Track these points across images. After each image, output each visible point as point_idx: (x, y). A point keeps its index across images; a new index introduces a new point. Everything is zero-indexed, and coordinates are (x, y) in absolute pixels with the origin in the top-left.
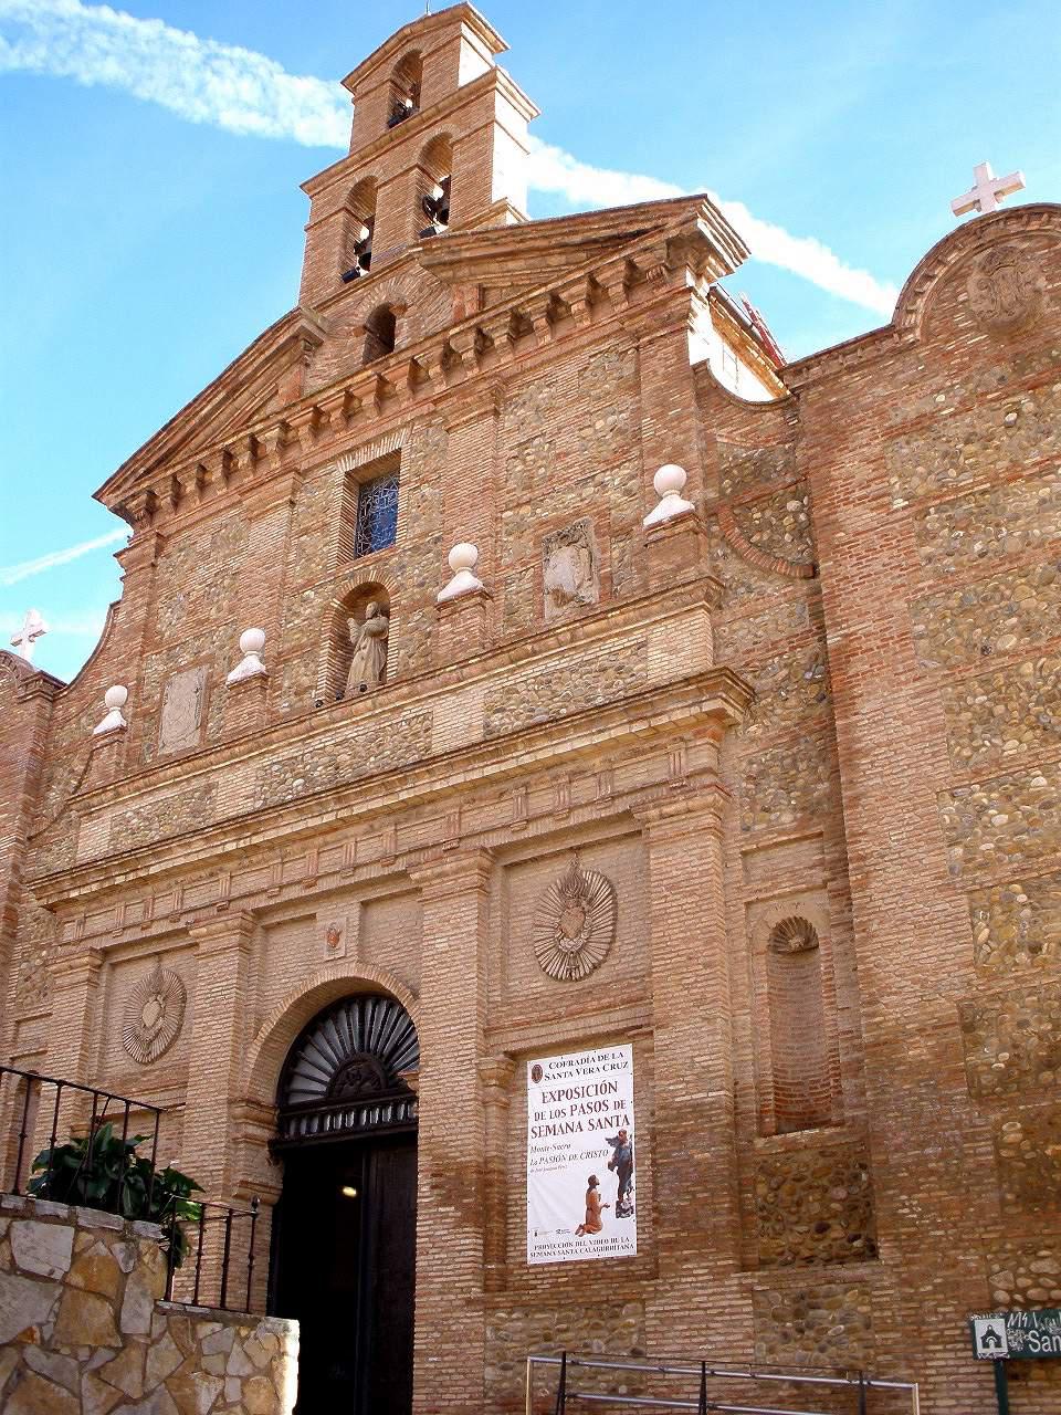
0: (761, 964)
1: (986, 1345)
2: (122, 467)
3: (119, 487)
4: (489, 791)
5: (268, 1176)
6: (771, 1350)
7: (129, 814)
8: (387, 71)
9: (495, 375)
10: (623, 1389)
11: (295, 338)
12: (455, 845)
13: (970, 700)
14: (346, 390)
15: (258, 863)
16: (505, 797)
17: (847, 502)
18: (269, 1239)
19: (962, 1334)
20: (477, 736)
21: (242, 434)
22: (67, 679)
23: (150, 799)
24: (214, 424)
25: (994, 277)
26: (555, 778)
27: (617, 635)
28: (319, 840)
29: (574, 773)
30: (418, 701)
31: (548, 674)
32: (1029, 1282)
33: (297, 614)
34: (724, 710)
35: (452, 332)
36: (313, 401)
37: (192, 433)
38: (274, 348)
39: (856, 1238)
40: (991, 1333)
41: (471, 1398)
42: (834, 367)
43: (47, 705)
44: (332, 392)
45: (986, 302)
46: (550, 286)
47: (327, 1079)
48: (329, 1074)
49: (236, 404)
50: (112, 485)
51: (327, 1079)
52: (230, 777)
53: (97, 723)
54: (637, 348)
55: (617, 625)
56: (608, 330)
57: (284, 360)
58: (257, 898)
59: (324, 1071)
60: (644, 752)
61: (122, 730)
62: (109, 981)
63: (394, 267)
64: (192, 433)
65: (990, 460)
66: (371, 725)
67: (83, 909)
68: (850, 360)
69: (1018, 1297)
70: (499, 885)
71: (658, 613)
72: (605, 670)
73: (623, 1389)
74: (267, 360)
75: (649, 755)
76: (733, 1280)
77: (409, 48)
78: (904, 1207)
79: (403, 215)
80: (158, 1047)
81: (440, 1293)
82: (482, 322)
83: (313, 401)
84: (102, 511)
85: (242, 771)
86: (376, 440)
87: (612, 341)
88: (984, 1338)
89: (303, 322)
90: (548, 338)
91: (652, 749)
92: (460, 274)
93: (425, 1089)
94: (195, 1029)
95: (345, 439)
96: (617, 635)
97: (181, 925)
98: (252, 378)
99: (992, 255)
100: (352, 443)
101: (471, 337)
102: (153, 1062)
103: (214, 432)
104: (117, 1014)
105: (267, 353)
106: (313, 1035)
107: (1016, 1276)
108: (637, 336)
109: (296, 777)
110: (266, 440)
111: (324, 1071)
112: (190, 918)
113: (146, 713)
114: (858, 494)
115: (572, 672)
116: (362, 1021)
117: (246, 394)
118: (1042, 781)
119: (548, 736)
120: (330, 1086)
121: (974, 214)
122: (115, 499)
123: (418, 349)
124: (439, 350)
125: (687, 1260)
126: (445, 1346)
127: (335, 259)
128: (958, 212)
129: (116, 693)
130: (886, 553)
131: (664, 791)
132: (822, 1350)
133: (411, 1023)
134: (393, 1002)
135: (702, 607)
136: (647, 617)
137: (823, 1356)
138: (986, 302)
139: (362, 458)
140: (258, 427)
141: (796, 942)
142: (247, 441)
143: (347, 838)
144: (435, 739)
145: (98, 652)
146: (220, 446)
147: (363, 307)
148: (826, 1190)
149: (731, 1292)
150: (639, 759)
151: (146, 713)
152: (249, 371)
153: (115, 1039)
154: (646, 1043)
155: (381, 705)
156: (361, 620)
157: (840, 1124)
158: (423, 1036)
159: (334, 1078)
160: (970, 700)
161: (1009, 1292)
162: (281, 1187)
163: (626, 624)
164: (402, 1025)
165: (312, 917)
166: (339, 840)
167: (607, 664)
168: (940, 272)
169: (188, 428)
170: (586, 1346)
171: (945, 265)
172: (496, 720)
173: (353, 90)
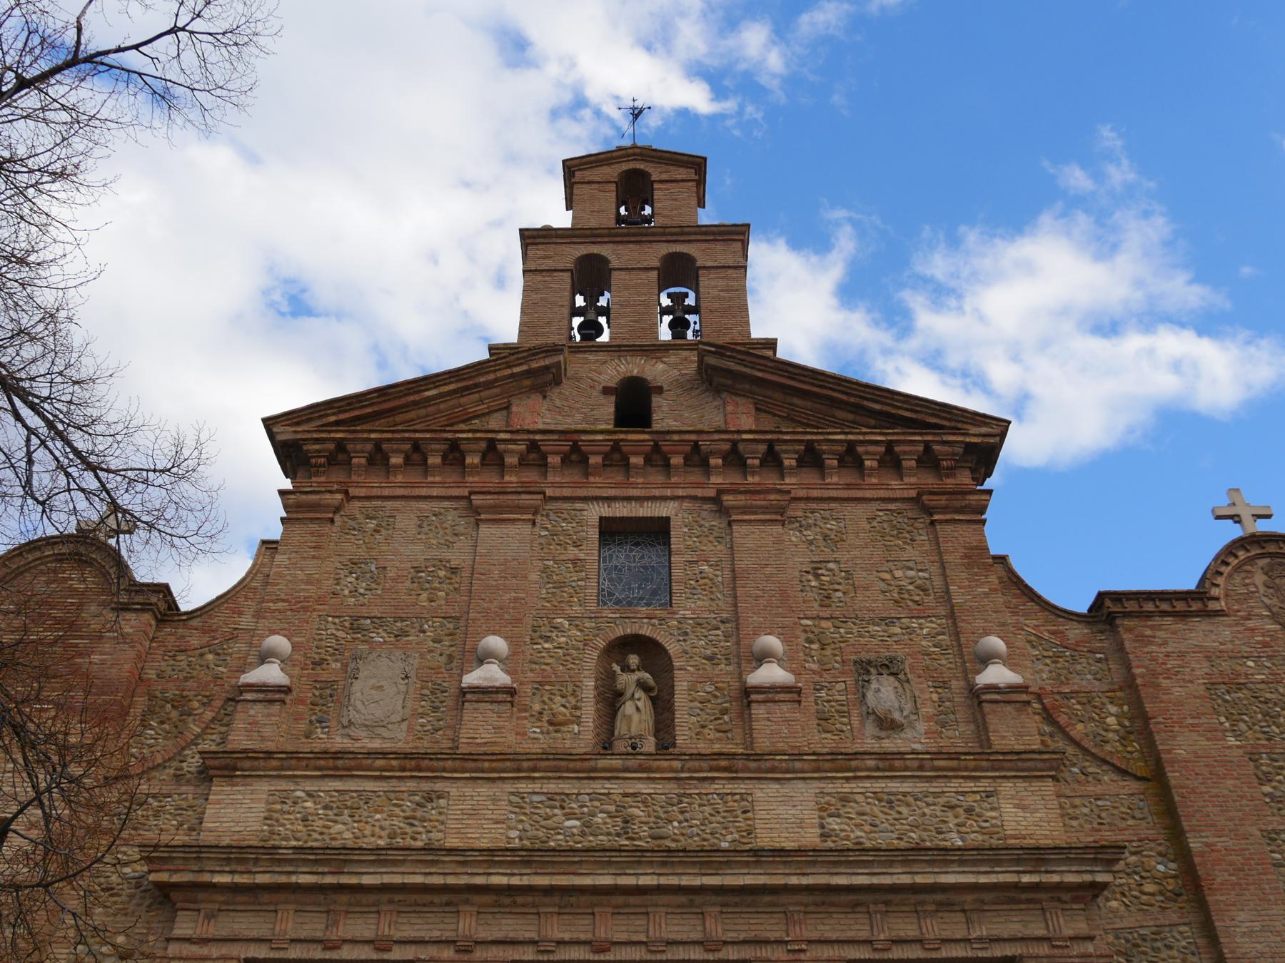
3: (298, 424)
4: (845, 898)
7: (299, 794)
12: (804, 947)
14: (616, 442)
15: (523, 905)
16: (859, 909)
21: (478, 435)
22: (184, 607)
23: (338, 785)
24: (430, 409)
26: (922, 903)
27: (963, 777)
28: (620, 899)
29: (940, 904)
30: (733, 778)
31: (889, 794)
33: (547, 639)
35: (745, 436)
36: (576, 437)
42: (1149, 607)
43: (153, 622)
44: (600, 437)
46: (851, 437)
52: (468, 790)
55: (966, 769)
56: (898, 494)
57: (527, 382)
58: (521, 948)
60: (1020, 902)
66: (672, 788)
67: (222, 898)
68: (1165, 606)
71: (1009, 770)
72: (952, 807)
74: (512, 375)
75: (1023, 906)
82: (778, 440)
83: (576, 437)
85: (484, 790)
86: (640, 499)
87: (899, 505)
90: (835, 479)
91: (1028, 901)
95: (600, 484)
96: (963, 777)
98: (489, 385)
100: (612, 492)
101: (762, 448)
103: (427, 416)
105: (516, 370)
109: (569, 816)
113: (321, 689)
115: (916, 800)
117: (477, 396)
119: (905, 862)
122: (286, 434)
123: (705, 437)
124: (726, 447)
136: (996, 770)
139: (621, 510)
142: (483, 445)
143: (657, 905)
146: (449, 436)
150: (1015, 907)
151: (321, 689)
152: (491, 377)
155: (689, 770)
163: (975, 770)
166: (646, 906)
167: (954, 802)
169: (403, 401)
172: (833, 824)
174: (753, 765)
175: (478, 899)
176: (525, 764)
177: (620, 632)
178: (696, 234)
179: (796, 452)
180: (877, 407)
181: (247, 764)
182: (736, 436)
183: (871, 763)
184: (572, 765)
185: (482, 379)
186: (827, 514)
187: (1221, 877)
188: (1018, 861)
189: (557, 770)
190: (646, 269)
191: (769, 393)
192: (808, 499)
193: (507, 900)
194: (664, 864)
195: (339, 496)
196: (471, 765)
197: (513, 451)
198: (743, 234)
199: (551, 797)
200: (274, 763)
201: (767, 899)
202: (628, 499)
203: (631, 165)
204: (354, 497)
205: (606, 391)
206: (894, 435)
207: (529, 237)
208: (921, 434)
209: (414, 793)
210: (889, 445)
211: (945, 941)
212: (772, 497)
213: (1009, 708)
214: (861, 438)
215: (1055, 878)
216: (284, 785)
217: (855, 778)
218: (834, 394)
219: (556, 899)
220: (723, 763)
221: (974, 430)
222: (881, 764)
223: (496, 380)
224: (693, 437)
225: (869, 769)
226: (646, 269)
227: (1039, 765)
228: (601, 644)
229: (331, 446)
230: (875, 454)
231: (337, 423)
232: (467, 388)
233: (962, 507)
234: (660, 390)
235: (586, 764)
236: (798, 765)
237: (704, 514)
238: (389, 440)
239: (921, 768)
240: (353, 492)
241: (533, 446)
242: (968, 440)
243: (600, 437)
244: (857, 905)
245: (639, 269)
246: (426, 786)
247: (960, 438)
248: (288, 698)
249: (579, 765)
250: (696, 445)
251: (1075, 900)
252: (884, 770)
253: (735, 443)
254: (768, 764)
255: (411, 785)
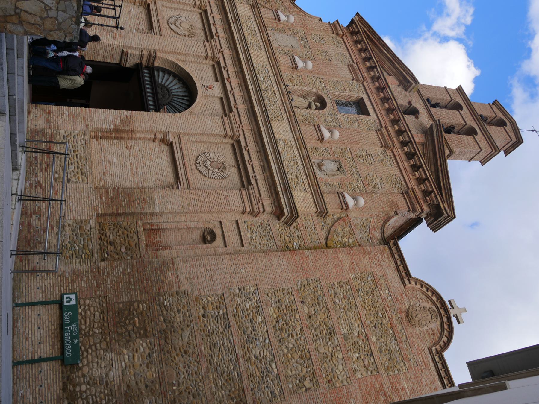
0: (201, 225)
1: (67, 298)
2: (367, 23)
3: (360, 22)
5: (130, 63)
6: (69, 225)
8: (500, 115)
9: (394, 147)
10: (57, 176)
11: (409, 81)
13: (287, 297)
17: (352, 259)
18: (109, 61)
19: (74, 289)
20: (277, 137)
25: (428, 312)
29: (264, 166)
32: (92, 312)
34: (284, 215)
36: (387, 87)
37: (377, 47)
38: (406, 75)
39: (108, 255)
40: (71, 300)
41: (53, 125)
44: (390, 93)
45: (419, 309)
47: (166, 85)
48: (167, 86)
49: (387, 62)
50: (361, 19)
51: (166, 85)
53: (281, 11)
54: (403, 193)
55: (312, 183)
56: (409, 184)
57: (401, 78)
59: (170, 84)
60: (270, 190)
61: (279, 20)
62: (196, 12)
63: (431, 115)
64: (377, 47)
65: (366, 307)
66: (280, 102)
69: (87, 307)
70: (227, 141)
73: (57, 176)
74: (401, 72)
76: (94, 214)
77: (508, 123)
78: (118, 270)
79: (449, 119)
80: (173, 27)
81: (90, 116)
82: (412, 143)
83: (387, 87)
84: (352, 16)
85: (266, 59)
87: (405, 185)
88: (69, 297)
89: (414, 84)
91: (271, 192)
92: (429, 136)
93: (159, 115)
94: (180, 39)
95: (375, 98)
97: (215, 37)
99: (435, 311)
102: (168, 25)
104: (185, 14)
105: (404, 72)
106: (183, 83)
107: (94, 307)
108: (407, 193)
109: (264, 77)
110: (374, 71)
111: (170, 84)
112: (217, 40)
114: (355, 262)
116: (178, 95)
117: (390, 65)
118: (260, 320)
120: (161, 84)
121: (449, 307)
122: (356, 19)
123: (404, 122)
125: (101, 198)
126: (72, 117)
127: (435, 97)
128: (450, 301)
129: (292, 19)
130: (335, 271)
131: (258, 196)
132: (69, 242)
133: (182, 111)
134: (189, 106)
135: (318, 210)
137: (67, 243)
138: (419, 309)
140: (379, 69)
141: (208, 237)
142: (373, 65)
144: (275, 122)
145: (305, 14)
146: (373, 56)
147: (418, 104)
148: (124, 245)
149: (90, 212)
151: (286, 29)
153: (176, 13)
154: (175, 187)
155: (287, 106)
156: (314, 101)
157: (147, 250)
158: (178, 114)
159: (166, 87)
160: (287, 297)
161: (89, 305)
162: (127, 66)
163: (312, 185)
164: (181, 109)
165: (217, 81)
167: (299, 179)
168: (430, 294)
169: (379, 45)
170: (71, 164)
171: (432, 296)
173: (494, 103)
174: (294, 121)
175: (234, 53)
176: (275, 67)
177: (326, 98)
178: (487, 136)
179: (410, 150)
180: (440, 175)
181: (256, 10)
182: (408, 131)
183: (305, 154)
184: (279, 77)
185: (396, 64)
186: (391, 162)
187: (297, 258)
188: (284, 184)
189: (276, 74)
190: (464, 120)
191: (430, 145)
192: (394, 156)
193: (236, 59)
194: (256, 90)
195: (342, 33)
196: (271, 55)
197: (375, 73)
198: (496, 151)
199: (268, 74)
200: (258, 15)
201: (253, 119)
202: (372, 105)
203: (505, 119)
204: (343, 39)
205: (410, 103)
206: (432, 178)
207: (460, 90)
208: (436, 188)
209: (259, 44)
210: (427, 179)
211: (252, 166)
212: (390, 142)
213: (339, 202)
214: (425, 169)
215: (281, 196)
216: (253, 18)
217: (298, 151)
218: (439, 161)
219: (239, 70)
220: (292, 114)
221: (446, 206)
222: (305, 156)
223: (398, 68)
224: (402, 119)
225: (302, 154)
226: (464, 120)
227: (320, 205)
228: (320, 93)
229: (357, 30)
230: (421, 175)
231: (365, 31)
232: (391, 61)
233: (412, 203)
234: (417, 117)
235: (280, 80)
236: (297, 133)
237: (376, 126)
238: (365, 42)
239: (307, 169)
240: (344, 37)
241: (379, 78)
242: (441, 204)
243: (390, 93)
244: (257, 143)
245: (463, 119)
246: (262, 47)
247: (440, 201)
248: (277, 21)
249: (279, 79)
250: (399, 120)
251: (276, 207)
252: (303, 158)
253: (405, 131)
254: (295, 125)
255: (262, 44)
